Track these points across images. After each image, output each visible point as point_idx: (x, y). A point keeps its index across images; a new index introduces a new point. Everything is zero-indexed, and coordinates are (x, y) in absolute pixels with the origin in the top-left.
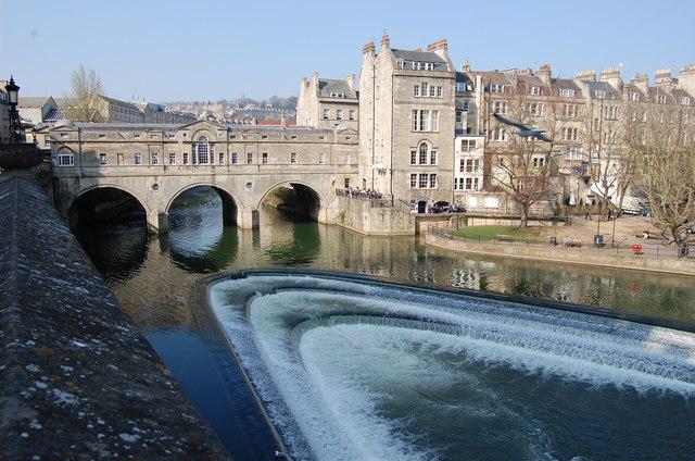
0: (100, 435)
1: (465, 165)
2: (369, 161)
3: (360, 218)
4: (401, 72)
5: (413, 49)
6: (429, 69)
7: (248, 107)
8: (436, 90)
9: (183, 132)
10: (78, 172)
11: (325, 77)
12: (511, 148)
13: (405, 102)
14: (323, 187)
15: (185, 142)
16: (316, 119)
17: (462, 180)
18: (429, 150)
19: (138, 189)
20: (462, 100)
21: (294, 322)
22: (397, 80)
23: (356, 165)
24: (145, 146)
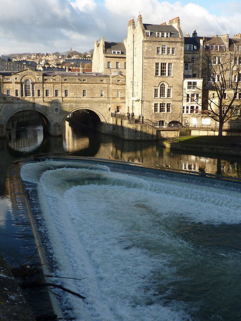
0: (7, 301)
2: (131, 95)
5: (159, 23)
6: (167, 37)
7: (74, 57)
11: (110, 41)
13: (150, 58)
15: (16, 83)
16: (103, 68)
17: (187, 108)
20: (190, 56)
22: (146, 44)
23: (123, 98)
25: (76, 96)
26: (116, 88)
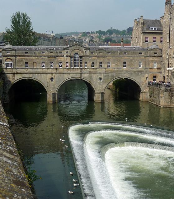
2: (167, 65)
3: (159, 97)
5: (155, 19)
9: (66, 51)
10: (14, 71)
14: (142, 81)
15: (67, 56)
19: (43, 80)
21: (104, 144)
24: (46, 58)
25: (117, 67)
26: (153, 60)
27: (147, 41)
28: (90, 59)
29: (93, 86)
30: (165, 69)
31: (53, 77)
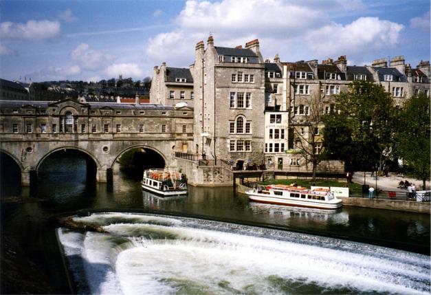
1: (274, 134)
2: (200, 130)
4: (222, 65)
5: (79, 80)
8: (249, 77)
9: (51, 108)
12: (40, 112)
15: (54, 116)
17: (271, 145)
18: (245, 122)
22: (219, 70)
23: (191, 134)
24: (20, 119)
27: (171, 97)
28: (90, 120)
29: (95, 160)
30: (311, 141)
31: (32, 146)
